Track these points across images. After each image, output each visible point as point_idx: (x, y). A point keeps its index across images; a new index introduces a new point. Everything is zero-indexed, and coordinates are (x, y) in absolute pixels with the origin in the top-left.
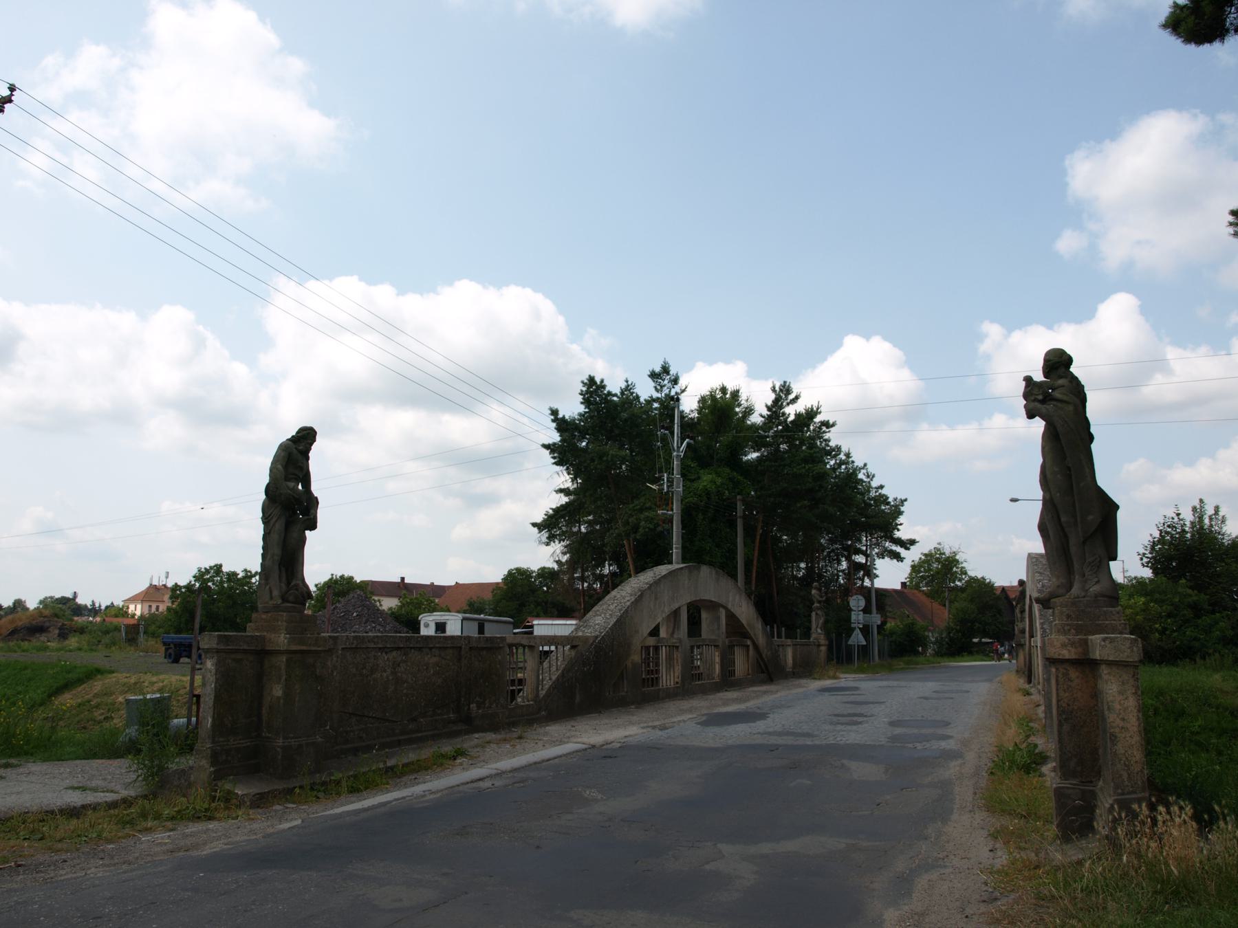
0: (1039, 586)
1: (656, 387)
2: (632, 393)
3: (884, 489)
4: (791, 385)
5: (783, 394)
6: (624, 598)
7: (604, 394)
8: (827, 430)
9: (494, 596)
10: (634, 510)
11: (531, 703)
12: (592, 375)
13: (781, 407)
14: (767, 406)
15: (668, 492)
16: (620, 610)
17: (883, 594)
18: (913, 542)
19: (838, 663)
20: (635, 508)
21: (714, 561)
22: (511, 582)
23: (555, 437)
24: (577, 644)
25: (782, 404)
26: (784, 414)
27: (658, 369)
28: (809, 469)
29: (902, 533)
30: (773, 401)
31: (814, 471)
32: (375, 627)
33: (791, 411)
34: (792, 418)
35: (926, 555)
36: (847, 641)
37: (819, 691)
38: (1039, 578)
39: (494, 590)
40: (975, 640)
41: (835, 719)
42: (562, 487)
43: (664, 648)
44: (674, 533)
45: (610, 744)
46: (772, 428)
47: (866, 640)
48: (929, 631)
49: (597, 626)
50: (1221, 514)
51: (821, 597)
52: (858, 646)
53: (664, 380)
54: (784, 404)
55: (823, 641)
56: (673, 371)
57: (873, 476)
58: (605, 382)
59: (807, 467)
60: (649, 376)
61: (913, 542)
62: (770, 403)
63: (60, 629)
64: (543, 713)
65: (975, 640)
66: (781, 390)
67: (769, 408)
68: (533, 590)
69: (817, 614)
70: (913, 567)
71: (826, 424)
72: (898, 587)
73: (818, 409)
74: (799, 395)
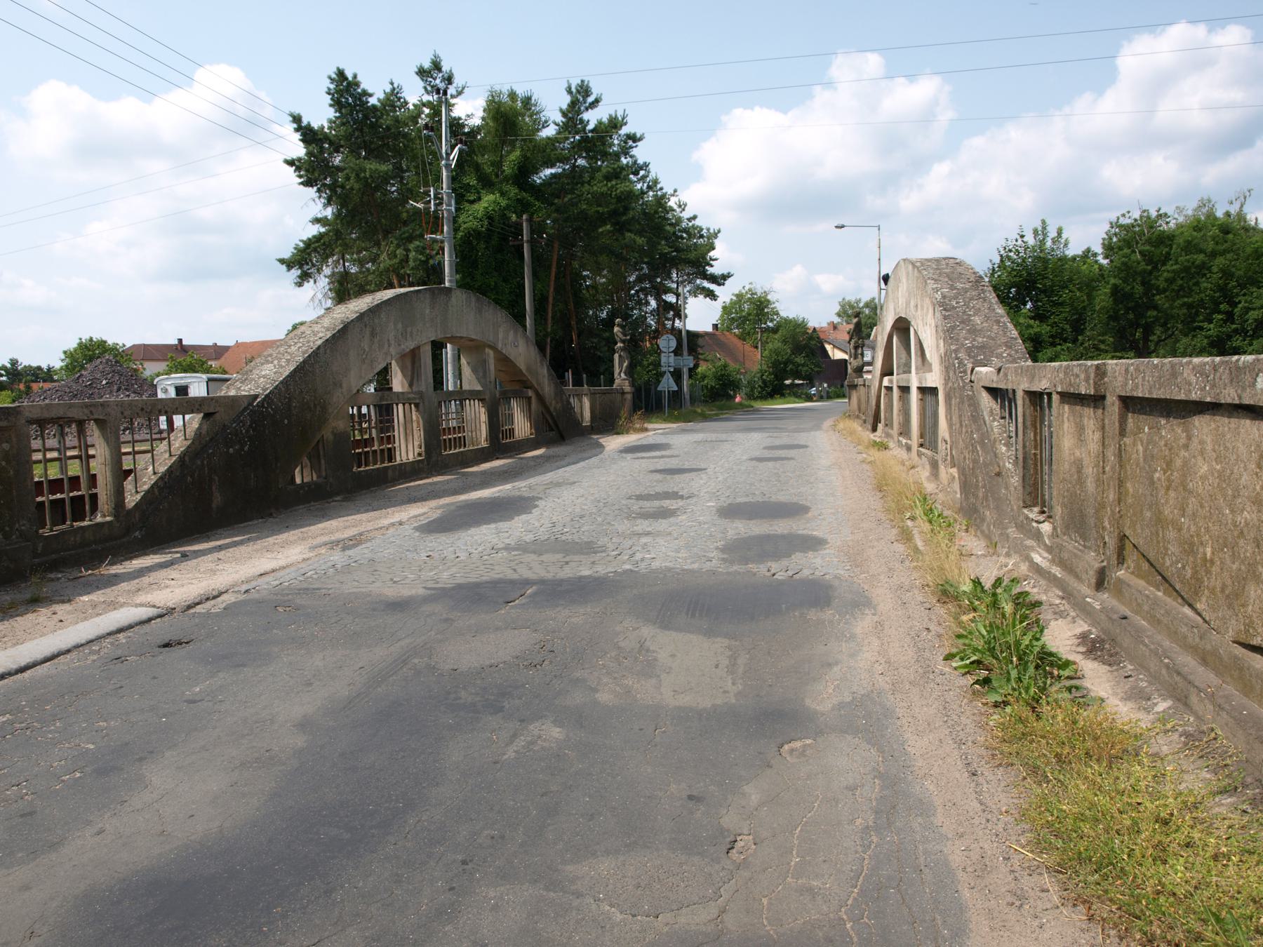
0: (938, 296)
1: (425, 88)
2: (399, 99)
3: (697, 220)
4: (590, 85)
5: (581, 97)
6: (315, 335)
7: (358, 93)
8: (634, 145)
10: (402, 239)
11: (108, 519)
12: (341, 68)
13: (579, 112)
14: (561, 110)
15: (436, 211)
16: (304, 353)
17: (693, 336)
18: (725, 277)
19: (647, 410)
20: (403, 236)
21: (501, 298)
23: (299, 150)
25: (579, 108)
26: (582, 121)
27: (427, 65)
28: (612, 187)
29: (716, 269)
30: (568, 105)
31: (617, 189)
33: (592, 118)
34: (591, 126)
35: (737, 296)
36: (656, 388)
37: (621, 452)
38: (935, 286)
40: (788, 382)
41: (636, 507)
42: (319, 216)
43: (400, 406)
44: (446, 263)
45: (215, 597)
46: (567, 138)
47: (677, 386)
48: (742, 373)
50: (1064, 236)
51: (625, 335)
52: (669, 391)
53: (435, 79)
54: (582, 108)
55: (627, 388)
56: (445, 68)
57: (685, 205)
58: (359, 78)
59: (609, 185)
60: (417, 73)
61: (725, 277)
62: (565, 107)
64: (137, 533)
65: (788, 382)
66: (578, 92)
67: (564, 114)
69: (620, 356)
70: (724, 308)
71: (634, 138)
72: (710, 329)
73: (623, 119)
74: (600, 98)
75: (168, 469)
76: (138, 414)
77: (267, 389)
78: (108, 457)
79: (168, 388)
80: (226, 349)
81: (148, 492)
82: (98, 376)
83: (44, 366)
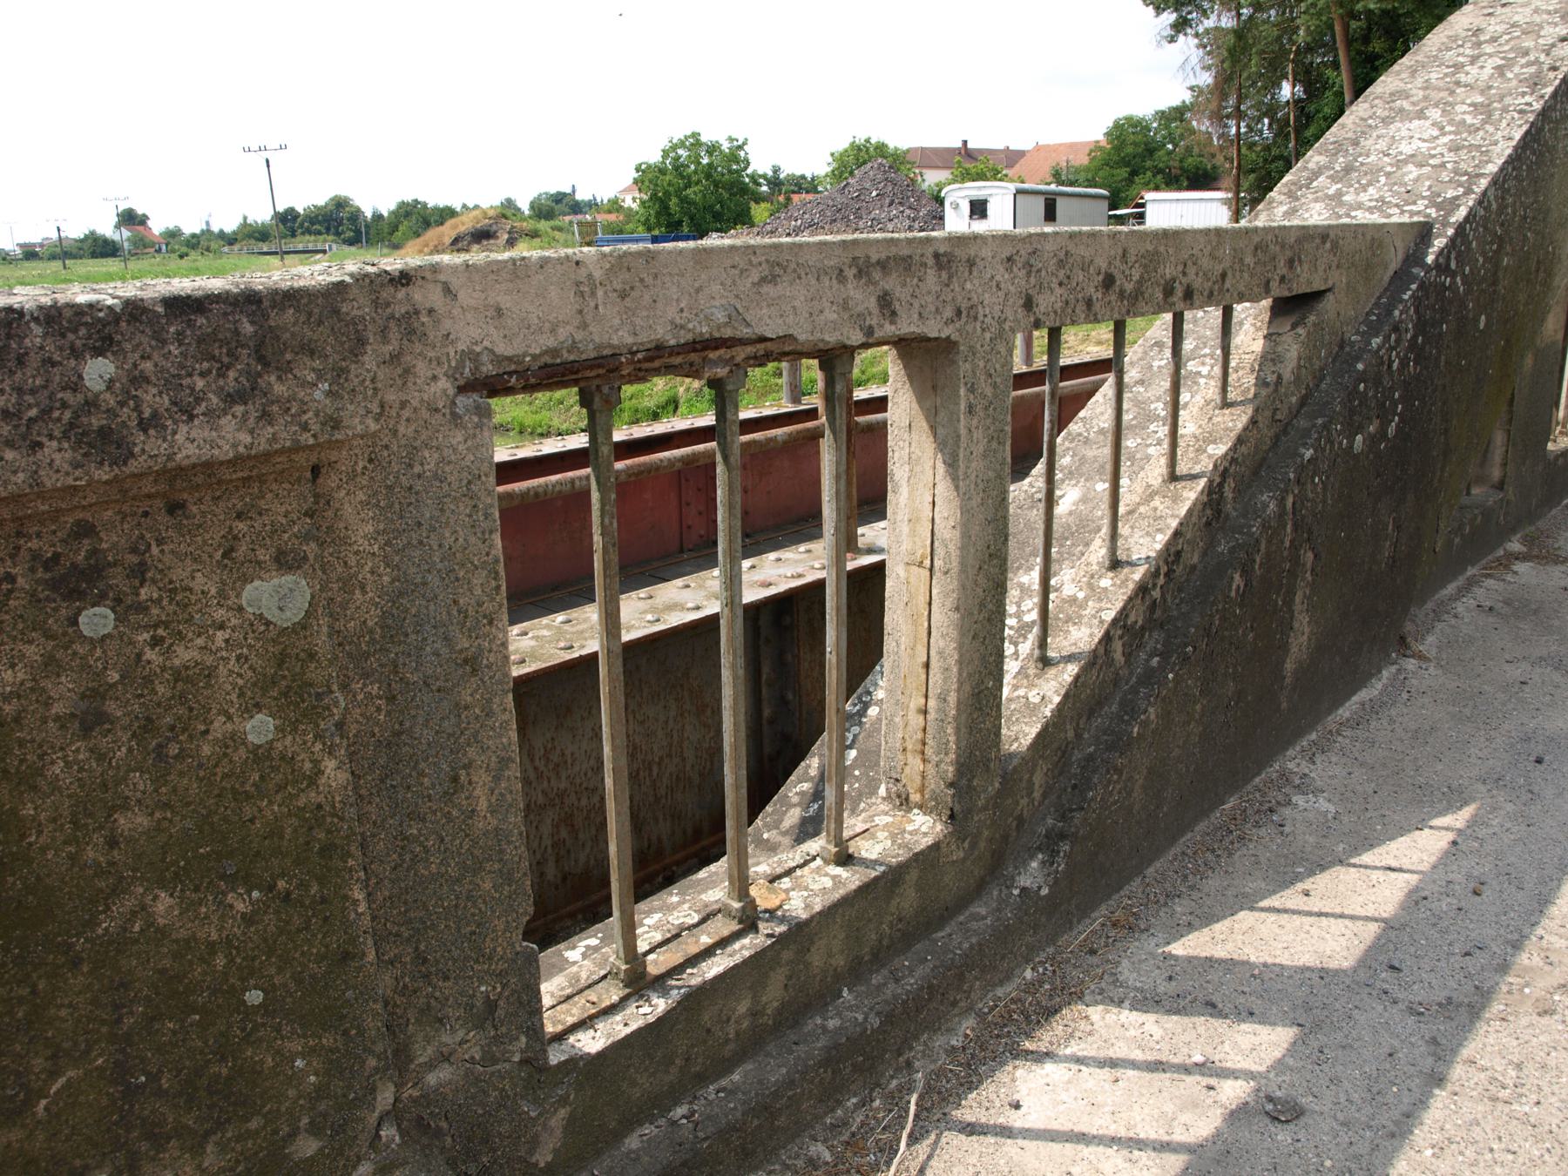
9: (1092, 160)
16: (1534, 83)
22: (1118, 138)
24: (1318, 286)
32: (902, 212)
39: (1091, 151)
49: (1412, 172)
63: (509, 233)
68: (1150, 150)
75: (1168, 545)
76: (1089, 303)
77: (1453, 203)
78: (948, 533)
79: (960, 201)
80: (1021, 154)
81: (1097, 660)
82: (867, 185)
83: (809, 176)
